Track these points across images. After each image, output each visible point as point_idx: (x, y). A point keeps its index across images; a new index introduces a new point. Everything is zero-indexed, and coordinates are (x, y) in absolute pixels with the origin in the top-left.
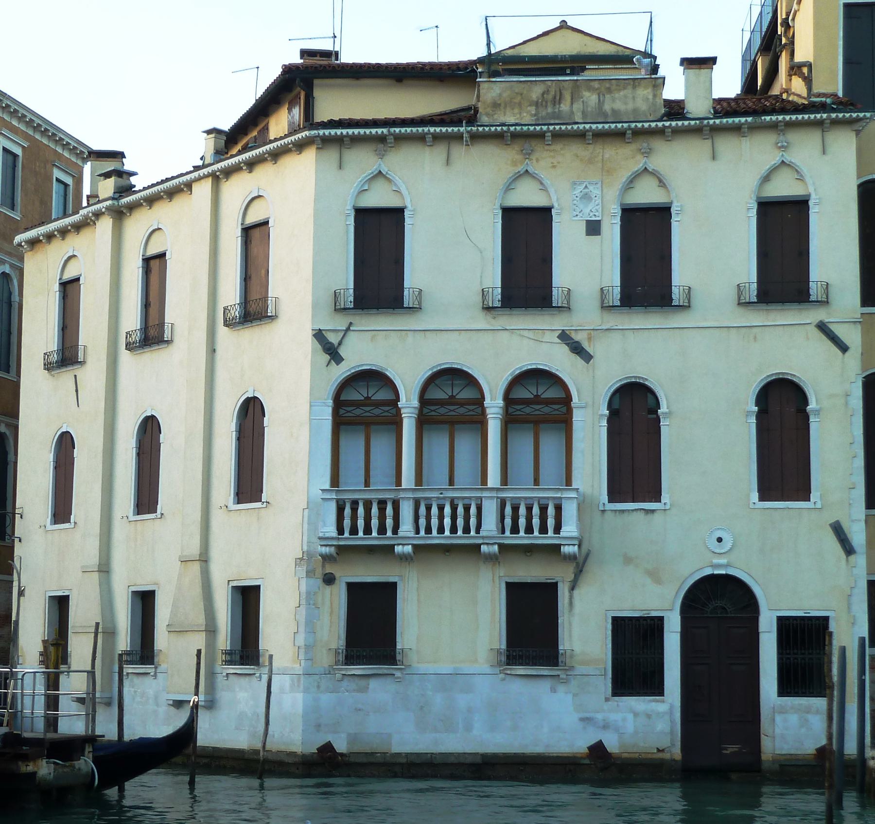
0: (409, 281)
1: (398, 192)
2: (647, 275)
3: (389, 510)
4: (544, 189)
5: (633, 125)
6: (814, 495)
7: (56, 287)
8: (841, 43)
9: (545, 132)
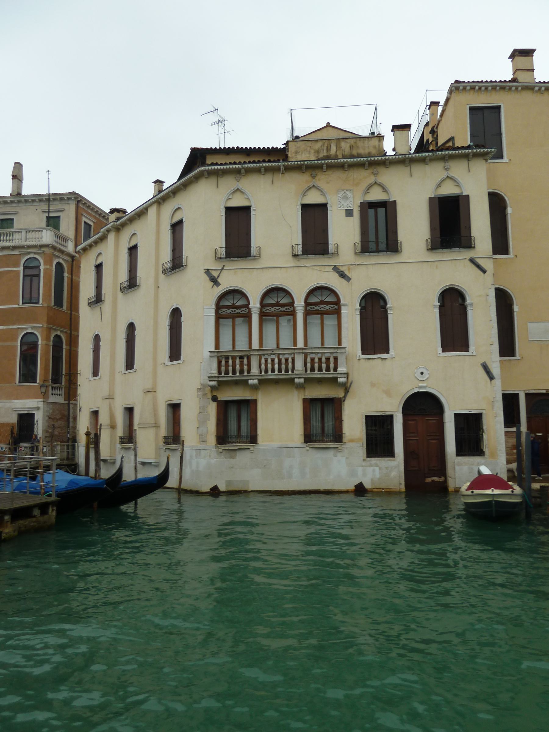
0: (254, 241)
1: (247, 198)
3: (245, 361)
5: (369, 159)
6: (472, 348)
7: (93, 268)
8: (469, 126)
9: (323, 164)
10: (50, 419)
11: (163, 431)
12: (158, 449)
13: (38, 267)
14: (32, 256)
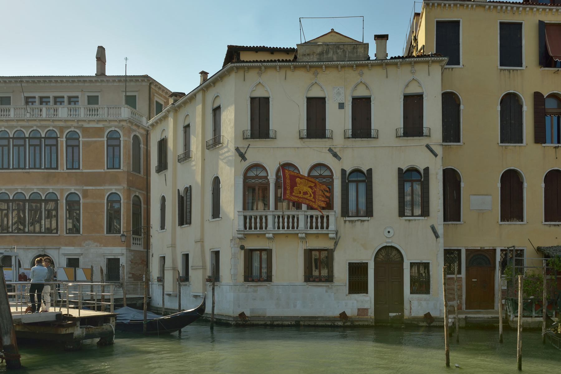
1: (267, 91)
2: (362, 127)
4: (323, 90)
9: (322, 65)
10: (132, 262)
11: (209, 273)
12: (204, 286)
13: (119, 139)
14: (113, 129)
